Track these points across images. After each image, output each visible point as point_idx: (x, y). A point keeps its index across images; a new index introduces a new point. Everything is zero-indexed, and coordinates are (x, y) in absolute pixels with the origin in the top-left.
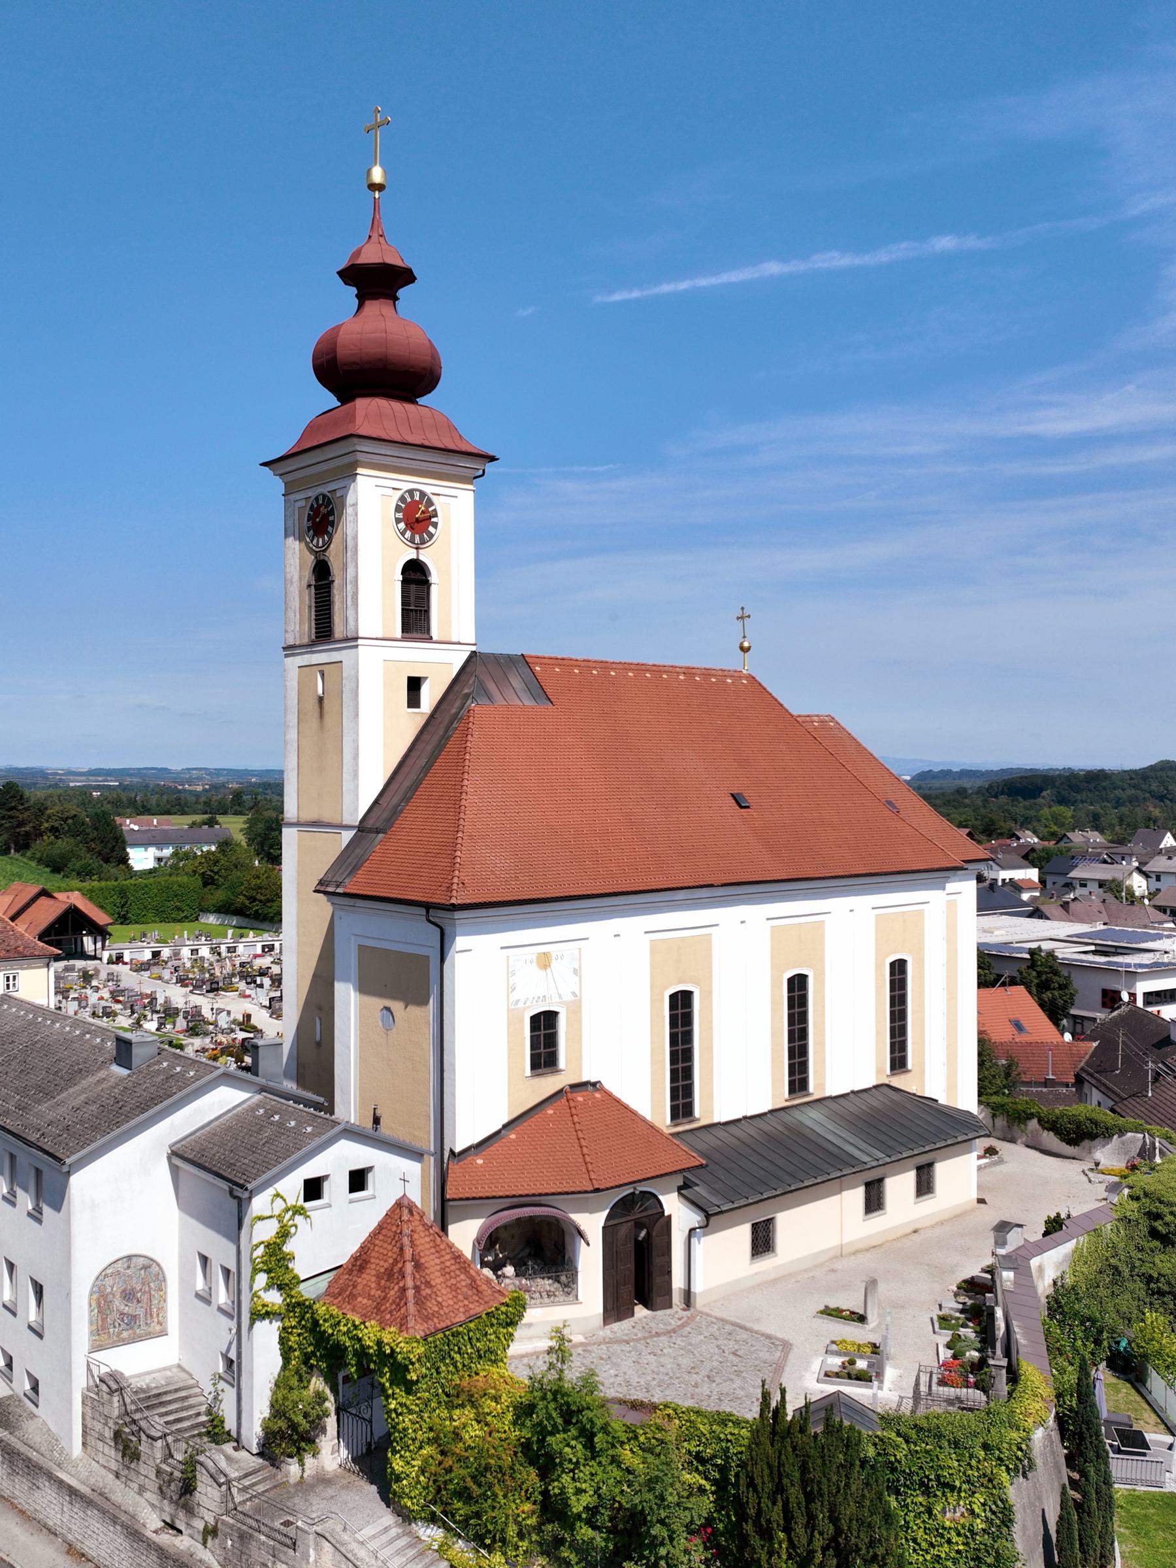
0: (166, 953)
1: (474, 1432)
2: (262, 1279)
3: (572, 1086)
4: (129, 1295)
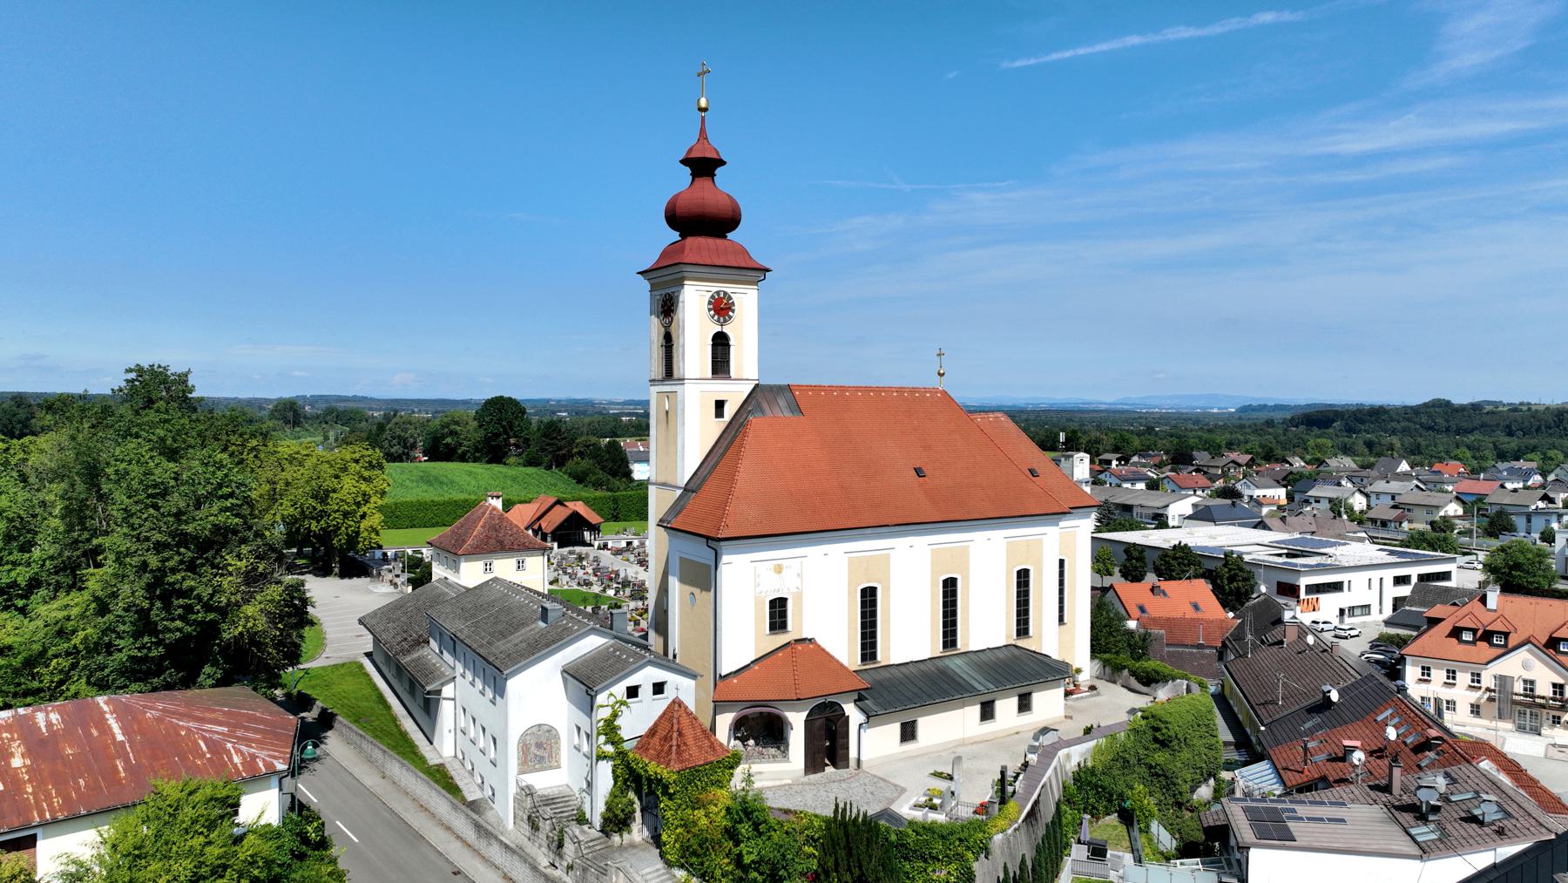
0: (636, 543)
1: (704, 821)
2: (602, 739)
3: (797, 641)
4: (539, 746)
